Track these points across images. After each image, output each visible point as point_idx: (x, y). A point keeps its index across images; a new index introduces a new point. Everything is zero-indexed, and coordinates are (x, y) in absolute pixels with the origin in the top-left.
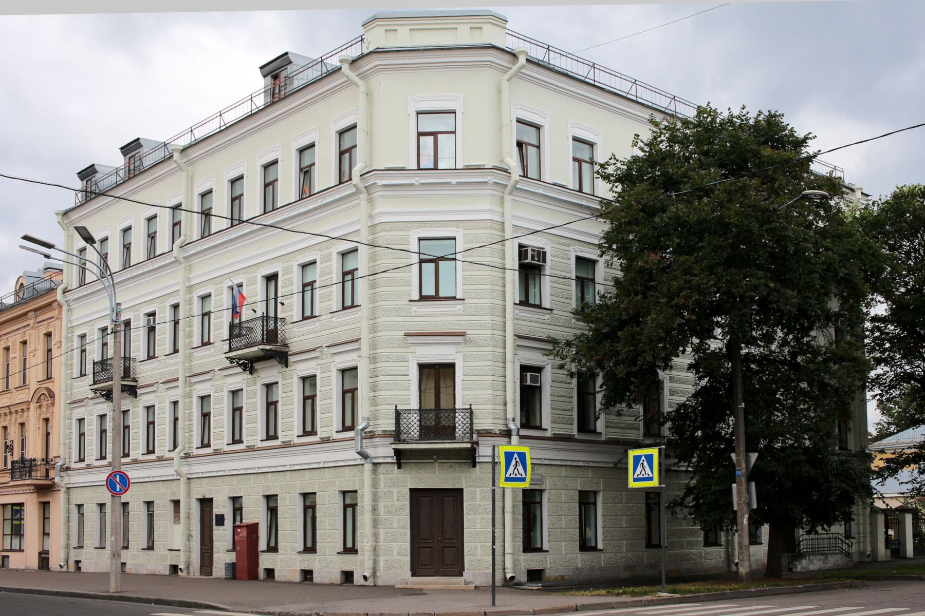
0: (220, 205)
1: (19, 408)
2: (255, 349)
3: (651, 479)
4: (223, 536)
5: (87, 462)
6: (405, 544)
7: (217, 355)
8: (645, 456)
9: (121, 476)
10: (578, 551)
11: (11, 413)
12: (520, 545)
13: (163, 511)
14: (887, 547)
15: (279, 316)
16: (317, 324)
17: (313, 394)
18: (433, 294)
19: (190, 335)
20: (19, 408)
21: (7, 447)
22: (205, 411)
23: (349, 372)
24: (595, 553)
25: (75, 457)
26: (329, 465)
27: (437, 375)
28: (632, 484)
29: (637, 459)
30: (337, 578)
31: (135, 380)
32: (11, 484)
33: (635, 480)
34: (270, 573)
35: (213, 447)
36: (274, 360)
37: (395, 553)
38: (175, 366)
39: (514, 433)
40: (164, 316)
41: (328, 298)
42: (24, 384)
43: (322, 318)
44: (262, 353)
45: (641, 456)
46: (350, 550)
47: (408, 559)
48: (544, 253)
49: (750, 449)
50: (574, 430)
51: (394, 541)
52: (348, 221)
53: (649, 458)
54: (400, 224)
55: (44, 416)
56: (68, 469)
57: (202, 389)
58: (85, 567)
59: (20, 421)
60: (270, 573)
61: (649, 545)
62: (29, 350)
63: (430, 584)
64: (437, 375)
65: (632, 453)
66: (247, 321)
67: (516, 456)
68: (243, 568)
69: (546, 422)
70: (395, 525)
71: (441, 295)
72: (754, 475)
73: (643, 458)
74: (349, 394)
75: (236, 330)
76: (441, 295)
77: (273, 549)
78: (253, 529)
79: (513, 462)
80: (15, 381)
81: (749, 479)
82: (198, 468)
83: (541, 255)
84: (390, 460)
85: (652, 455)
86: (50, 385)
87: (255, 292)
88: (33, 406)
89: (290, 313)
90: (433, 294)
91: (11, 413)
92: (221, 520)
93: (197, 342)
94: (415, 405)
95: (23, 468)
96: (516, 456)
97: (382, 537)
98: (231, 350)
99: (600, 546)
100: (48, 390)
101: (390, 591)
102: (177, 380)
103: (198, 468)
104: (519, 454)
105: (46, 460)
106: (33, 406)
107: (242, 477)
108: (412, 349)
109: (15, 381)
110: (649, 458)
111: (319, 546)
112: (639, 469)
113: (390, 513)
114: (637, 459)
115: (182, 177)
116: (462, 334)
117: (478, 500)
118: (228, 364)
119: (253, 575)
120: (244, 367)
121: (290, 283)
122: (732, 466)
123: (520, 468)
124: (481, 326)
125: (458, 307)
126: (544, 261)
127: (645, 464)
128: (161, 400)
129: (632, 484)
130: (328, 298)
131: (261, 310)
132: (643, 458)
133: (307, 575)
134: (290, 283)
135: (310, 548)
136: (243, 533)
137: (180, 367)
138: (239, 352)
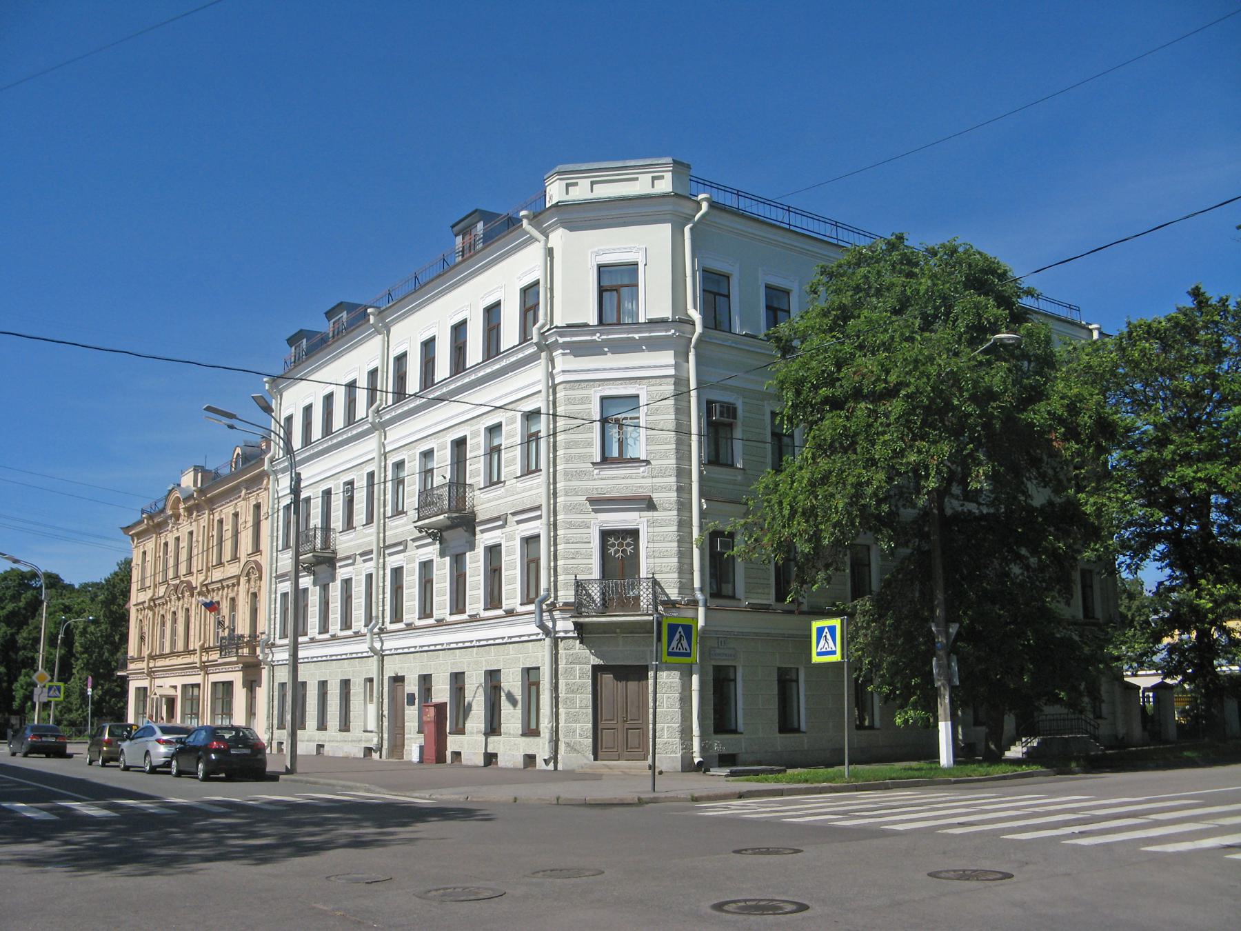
0: (387, 382)
1: (230, 582)
2: (441, 517)
3: (834, 653)
5: (354, 629)
7: (403, 527)
11: (208, 591)
12: (710, 723)
13: (357, 690)
14: (1144, 728)
20: (230, 582)
21: (219, 622)
23: (530, 542)
24: (737, 736)
26: (511, 641)
28: (816, 659)
30: (520, 762)
31: (334, 552)
32: (220, 661)
33: (819, 654)
34: (457, 755)
35: (468, 613)
36: (460, 529)
38: (364, 537)
39: (701, 603)
40: (361, 483)
41: (512, 461)
42: (235, 558)
45: (823, 628)
48: (735, 409)
49: (949, 619)
50: (770, 600)
51: (575, 722)
52: (527, 384)
53: (832, 630)
55: (252, 590)
56: (273, 645)
57: (393, 561)
58: (328, 750)
59: (231, 595)
60: (457, 755)
61: (783, 729)
62: (240, 521)
65: (816, 625)
66: (438, 487)
67: (680, 629)
68: (431, 752)
69: (740, 591)
72: (952, 649)
74: (531, 566)
75: (426, 496)
78: (440, 708)
79: (677, 636)
80: (227, 555)
82: (390, 644)
83: (730, 410)
84: (571, 634)
85: (230, 683)
86: (258, 558)
87: (443, 458)
88: (243, 580)
89: (477, 479)
91: (223, 588)
94: (596, 574)
95: (230, 643)
96: (680, 629)
98: (419, 519)
99: (803, 727)
100: (256, 562)
101: (571, 775)
102: (371, 552)
103: (390, 644)
104: (683, 626)
105: (254, 635)
106: (243, 580)
107: (434, 650)
109: (227, 555)
110: (832, 630)
112: (822, 641)
114: (820, 631)
115: (378, 340)
118: (417, 534)
119: (440, 758)
120: (434, 536)
121: (476, 448)
122: (930, 637)
123: (685, 643)
126: (735, 417)
127: (828, 636)
128: (356, 572)
129: (816, 659)
130: (512, 461)
133: (490, 758)
134: (476, 448)
136: (432, 711)
137: (374, 538)
138: (427, 521)
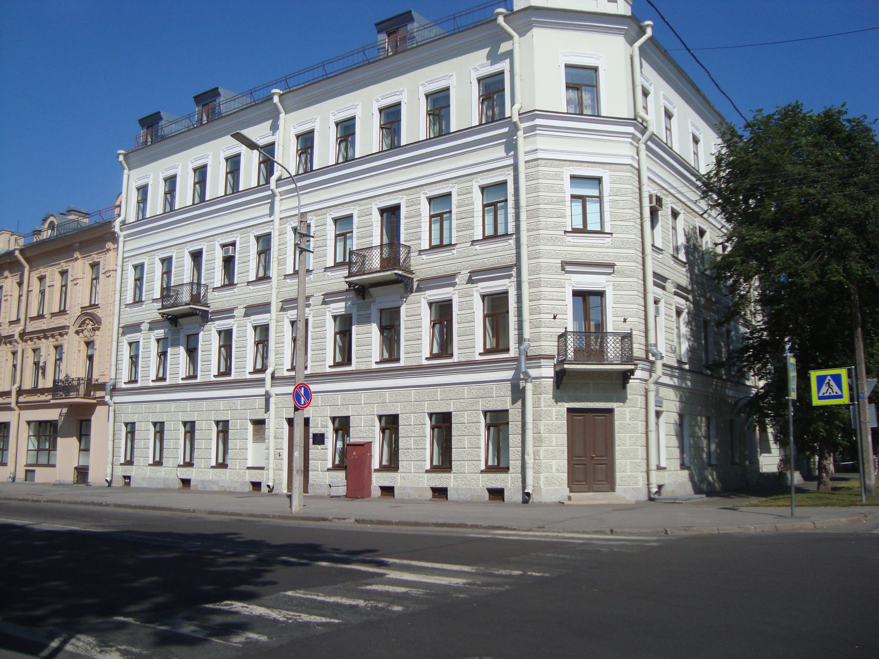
3: (841, 397)
4: (324, 456)
6: (562, 463)
8: (831, 376)
9: (305, 389)
10: (678, 468)
15: (203, 282)
16: (454, 251)
17: (347, 328)
18: (581, 227)
19: (282, 263)
22: (191, 347)
25: (125, 376)
27: (588, 301)
29: (821, 380)
31: (206, 305)
32: (52, 402)
33: (820, 398)
37: (554, 470)
43: (458, 246)
44: (395, 277)
46: (130, 463)
47: (565, 476)
51: (553, 458)
53: (837, 379)
54: (555, 162)
63: (592, 499)
64: (588, 301)
70: (554, 444)
71: (589, 228)
73: (829, 378)
76: (589, 228)
77: (392, 465)
78: (365, 447)
81: (870, 402)
90: (581, 227)
92: (319, 439)
93: (130, 300)
97: (542, 455)
108: (568, 276)
111: (135, 460)
112: (824, 388)
113: (550, 432)
116: (612, 266)
117: (627, 419)
124: (627, 260)
125: (608, 240)
127: (832, 383)
129: (816, 402)
131: (187, 279)
132: (829, 378)
135: (445, 464)
